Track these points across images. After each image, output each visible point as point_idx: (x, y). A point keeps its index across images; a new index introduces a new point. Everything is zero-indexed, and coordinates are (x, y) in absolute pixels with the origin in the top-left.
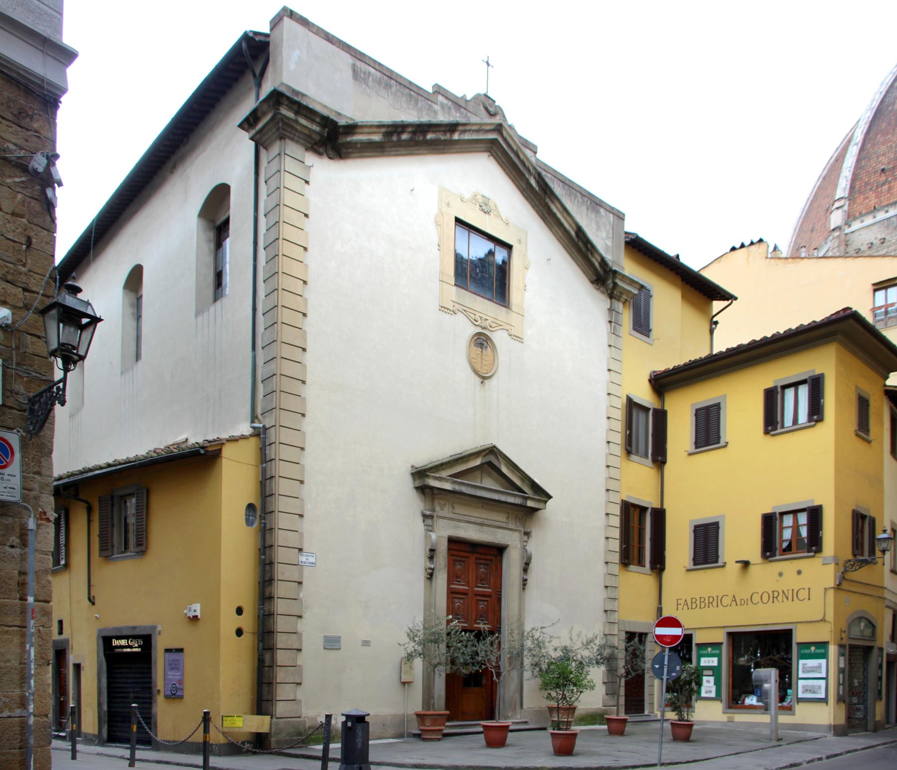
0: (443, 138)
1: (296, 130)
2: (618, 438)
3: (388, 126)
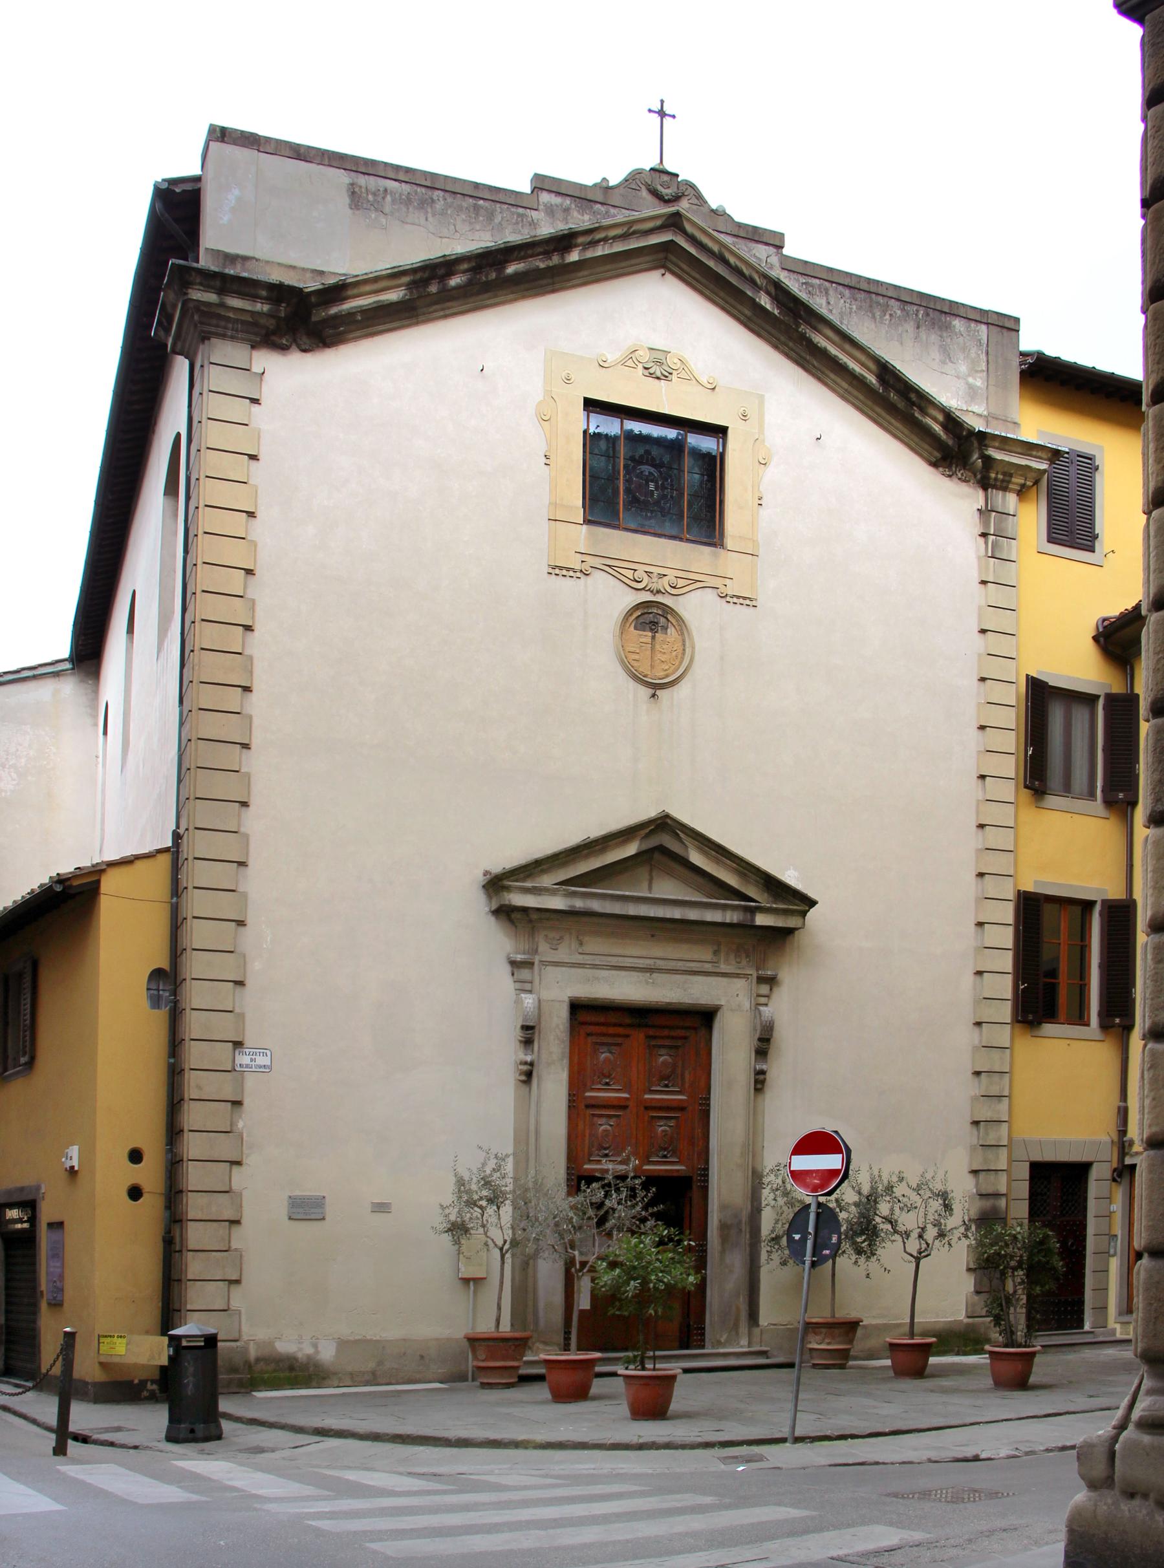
0: (542, 265)
1: (228, 319)
2: (1009, 766)
3: (414, 271)
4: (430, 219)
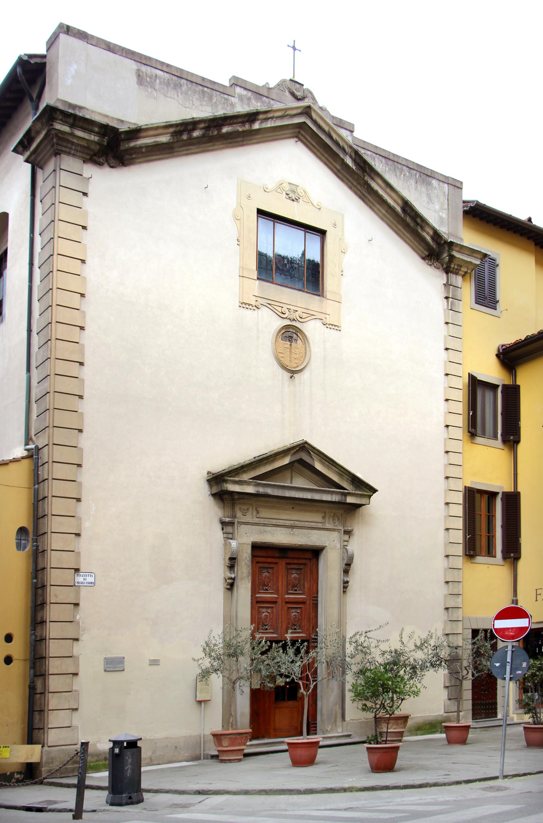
1: (73, 143)
2: (460, 421)
3: (177, 125)
4: (180, 96)
